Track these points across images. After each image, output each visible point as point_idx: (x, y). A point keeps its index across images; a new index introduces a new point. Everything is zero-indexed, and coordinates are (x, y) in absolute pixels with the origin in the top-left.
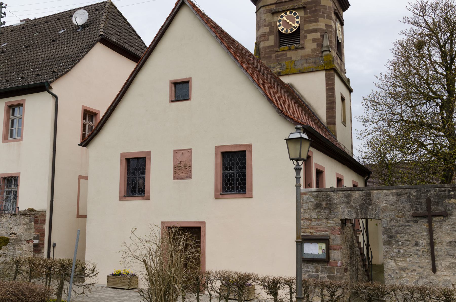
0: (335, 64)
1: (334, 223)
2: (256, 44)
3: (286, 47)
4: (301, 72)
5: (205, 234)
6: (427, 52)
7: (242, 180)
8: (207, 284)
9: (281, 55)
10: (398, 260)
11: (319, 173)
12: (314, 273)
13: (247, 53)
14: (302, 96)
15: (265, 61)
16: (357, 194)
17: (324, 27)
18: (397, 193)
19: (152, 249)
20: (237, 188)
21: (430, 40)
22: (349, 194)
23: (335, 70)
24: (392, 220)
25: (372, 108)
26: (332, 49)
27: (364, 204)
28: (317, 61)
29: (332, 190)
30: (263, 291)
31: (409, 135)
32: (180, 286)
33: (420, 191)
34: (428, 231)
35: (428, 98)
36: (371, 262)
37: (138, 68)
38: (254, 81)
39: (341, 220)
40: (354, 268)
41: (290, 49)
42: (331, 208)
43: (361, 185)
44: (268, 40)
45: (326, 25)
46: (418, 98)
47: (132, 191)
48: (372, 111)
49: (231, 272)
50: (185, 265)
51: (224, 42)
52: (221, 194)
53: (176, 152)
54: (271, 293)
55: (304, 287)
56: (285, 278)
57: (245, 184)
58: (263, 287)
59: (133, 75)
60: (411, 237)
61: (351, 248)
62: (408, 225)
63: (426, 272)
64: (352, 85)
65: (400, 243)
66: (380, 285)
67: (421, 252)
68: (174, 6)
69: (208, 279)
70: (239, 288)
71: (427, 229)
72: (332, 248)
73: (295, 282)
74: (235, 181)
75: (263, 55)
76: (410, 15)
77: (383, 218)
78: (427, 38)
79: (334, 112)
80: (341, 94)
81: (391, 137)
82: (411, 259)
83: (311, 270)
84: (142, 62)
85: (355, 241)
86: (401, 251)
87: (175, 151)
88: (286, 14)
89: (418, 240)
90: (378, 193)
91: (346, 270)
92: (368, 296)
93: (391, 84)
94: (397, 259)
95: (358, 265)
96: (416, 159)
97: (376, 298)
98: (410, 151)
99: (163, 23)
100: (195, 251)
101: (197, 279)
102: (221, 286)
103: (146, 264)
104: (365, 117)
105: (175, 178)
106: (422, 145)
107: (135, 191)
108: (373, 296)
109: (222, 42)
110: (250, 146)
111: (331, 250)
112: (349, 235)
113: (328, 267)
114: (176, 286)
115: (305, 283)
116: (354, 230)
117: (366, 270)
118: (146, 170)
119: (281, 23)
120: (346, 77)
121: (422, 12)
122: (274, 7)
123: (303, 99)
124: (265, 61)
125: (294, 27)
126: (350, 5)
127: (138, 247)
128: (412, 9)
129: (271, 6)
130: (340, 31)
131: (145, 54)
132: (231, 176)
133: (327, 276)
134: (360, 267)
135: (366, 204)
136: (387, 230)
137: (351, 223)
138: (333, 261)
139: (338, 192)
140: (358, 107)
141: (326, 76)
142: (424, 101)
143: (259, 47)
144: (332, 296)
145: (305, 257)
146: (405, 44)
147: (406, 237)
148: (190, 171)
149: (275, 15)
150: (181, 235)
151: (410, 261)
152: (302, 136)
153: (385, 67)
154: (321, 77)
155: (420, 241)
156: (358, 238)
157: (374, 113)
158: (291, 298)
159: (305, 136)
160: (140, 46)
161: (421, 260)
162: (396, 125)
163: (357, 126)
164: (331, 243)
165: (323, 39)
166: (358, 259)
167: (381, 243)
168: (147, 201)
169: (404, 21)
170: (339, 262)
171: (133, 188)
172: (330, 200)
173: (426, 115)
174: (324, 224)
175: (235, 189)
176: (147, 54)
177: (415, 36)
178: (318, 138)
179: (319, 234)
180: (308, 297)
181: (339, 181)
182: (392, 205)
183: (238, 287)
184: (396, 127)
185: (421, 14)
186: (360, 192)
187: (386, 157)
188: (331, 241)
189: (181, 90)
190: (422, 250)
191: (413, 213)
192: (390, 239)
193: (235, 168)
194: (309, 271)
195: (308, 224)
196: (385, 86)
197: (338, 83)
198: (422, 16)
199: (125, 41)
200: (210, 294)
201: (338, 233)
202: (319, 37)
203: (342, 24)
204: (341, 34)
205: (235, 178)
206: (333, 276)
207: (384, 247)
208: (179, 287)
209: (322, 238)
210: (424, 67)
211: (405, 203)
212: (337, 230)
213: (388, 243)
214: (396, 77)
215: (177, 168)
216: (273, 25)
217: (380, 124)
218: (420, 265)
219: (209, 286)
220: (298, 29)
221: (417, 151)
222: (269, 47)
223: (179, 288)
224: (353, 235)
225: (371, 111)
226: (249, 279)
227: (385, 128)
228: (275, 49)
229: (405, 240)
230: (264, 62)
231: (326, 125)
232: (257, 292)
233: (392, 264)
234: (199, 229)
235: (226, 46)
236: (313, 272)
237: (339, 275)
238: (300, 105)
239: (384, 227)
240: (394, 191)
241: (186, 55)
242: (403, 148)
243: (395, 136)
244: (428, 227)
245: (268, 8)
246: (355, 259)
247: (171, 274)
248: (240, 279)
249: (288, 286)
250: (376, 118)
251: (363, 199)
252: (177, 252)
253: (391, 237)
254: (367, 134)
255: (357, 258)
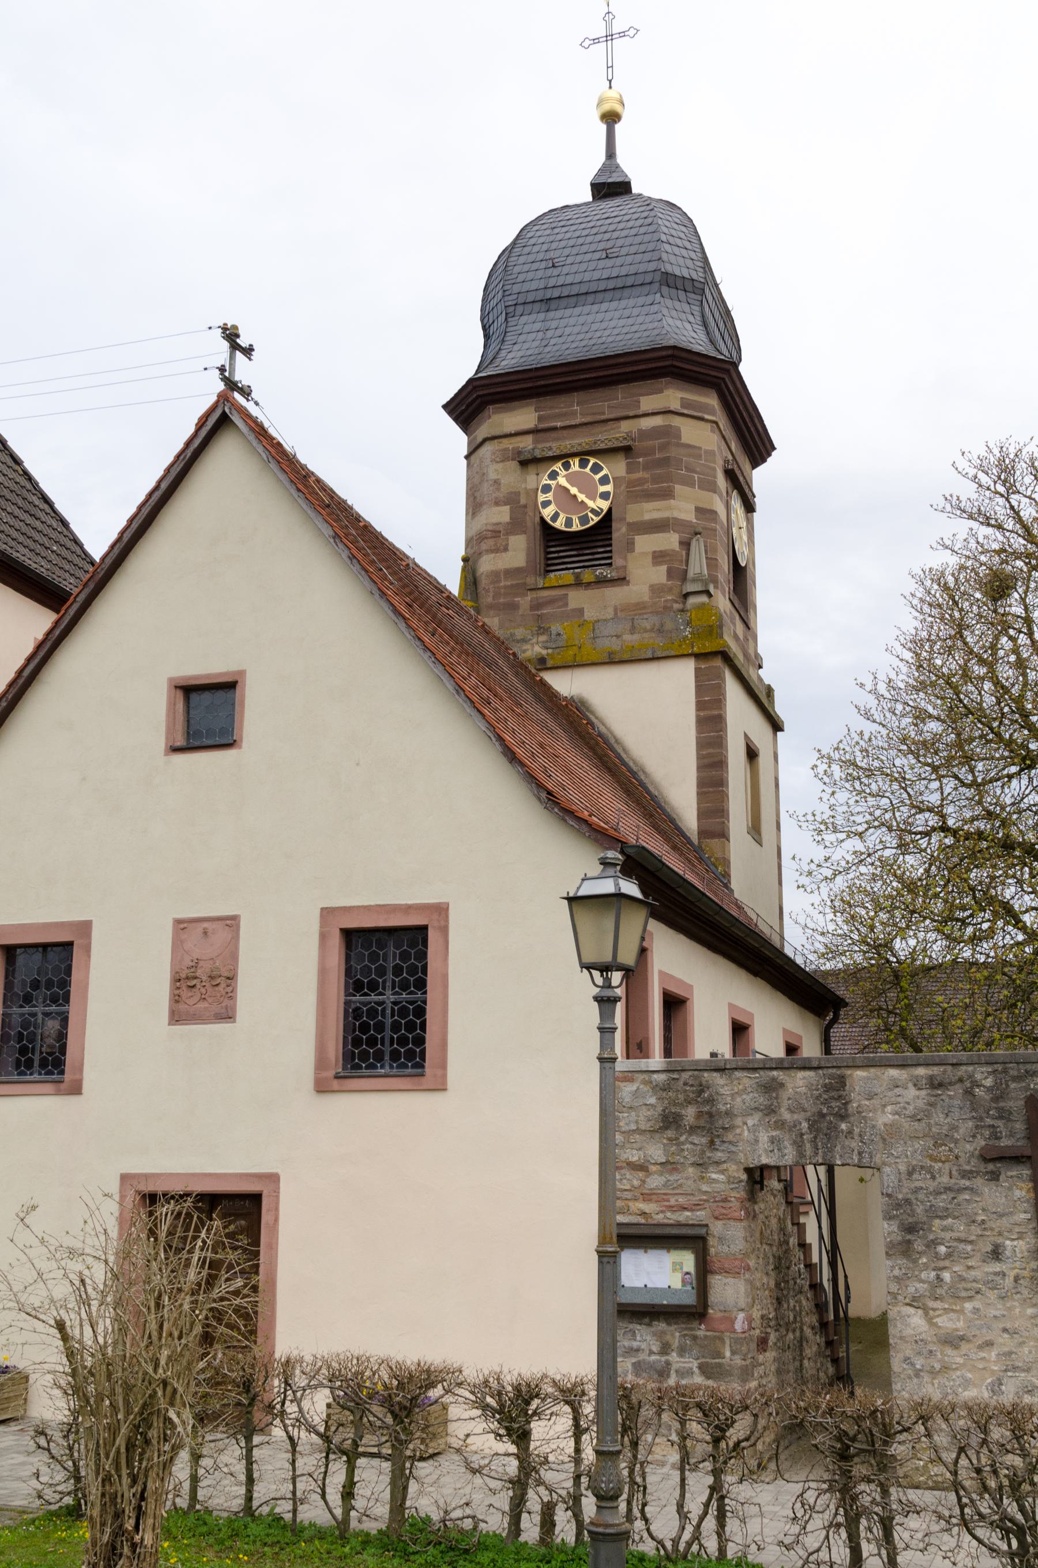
0: (726, 637)
1: (724, 1180)
2: (465, 560)
3: (567, 577)
4: (613, 660)
5: (276, 1220)
6: (1019, 610)
7: (411, 1027)
8: (283, 1404)
9: (552, 601)
10: (934, 1310)
11: (674, 1004)
12: (653, 1358)
13: (435, 591)
14: (617, 741)
15: (496, 620)
16: (799, 1082)
17: (690, 517)
18: (931, 1078)
19: (88, 1281)
20: (395, 1056)
21: (1030, 572)
22: (774, 1079)
23: (726, 657)
24: (914, 1169)
25: (847, 785)
26: (716, 587)
27: (823, 1116)
28: (669, 625)
29: (716, 1066)
30: (480, 1426)
31: (966, 880)
32: (187, 1414)
33: (1005, 1071)
34: (1032, 1209)
35: (1024, 759)
36: (846, 1313)
37: (57, 632)
38: (459, 689)
39: (748, 1171)
40: (791, 1336)
41: (578, 584)
42: (713, 1126)
43: (811, 1048)
44: (506, 549)
45: (699, 510)
46: (993, 758)
47: (18, 1064)
48: (847, 795)
49: (368, 1359)
50: (207, 1339)
51: (359, 556)
52: (337, 1077)
53: (181, 925)
54: (509, 1435)
55: (621, 1409)
56: (558, 1377)
57: (420, 1041)
58: (479, 1412)
59: (41, 654)
60: (976, 1230)
61: (781, 1265)
62: (966, 1189)
63: (1026, 1350)
64: (780, 708)
65: (942, 1249)
66: (879, 1402)
67: (1009, 1282)
68: (192, 430)
69: (287, 1383)
70: (395, 1416)
71: (1028, 1201)
72: (716, 1266)
73: (593, 1393)
74: (388, 1032)
75: (490, 600)
76: (967, 491)
77: (884, 1164)
78: (1019, 563)
79: (723, 797)
80: (746, 736)
81: (911, 887)
82: (977, 1304)
83: (644, 1346)
84: (72, 612)
85: (793, 1241)
86: (946, 1276)
87: (178, 922)
88: (567, 466)
89: (1000, 1240)
90: (868, 1078)
91: (762, 1344)
92: (839, 1439)
93: (908, 709)
94: (931, 1304)
95: (802, 1324)
96: (988, 956)
97: (865, 1447)
98: (970, 930)
99: (152, 484)
100: (245, 1286)
101: (247, 1386)
102: (329, 1406)
103: (65, 1338)
104: (825, 817)
105: (176, 1017)
106: (1011, 915)
107: (29, 1064)
108: (854, 1439)
109: (352, 557)
110: (441, 910)
111: (712, 1272)
112: (774, 1221)
113: (701, 1333)
114: (172, 1414)
115: (626, 1397)
116: (789, 1203)
117: (829, 1343)
118: (73, 989)
119: (550, 496)
120: (760, 679)
121: (1005, 482)
122: (526, 443)
123: (620, 751)
124: (496, 620)
125: (593, 511)
126: (774, 448)
127: (40, 1274)
128: (972, 472)
129: (519, 439)
130: (744, 531)
131: (85, 585)
132: (372, 1013)
133: (700, 1367)
134: (808, 1331)
135: (831, 1116)
136: (898, 1206)
137: (780, 1181)
138: (719, 1315)
139: (738, 1074)
140: (799, 779)
141: (696, 677)
142: (1014, 769)
143: (474, 572)
144: (716, 1441)
145: (624, 1298)
146: (951, 580)
147: (961, 1228)
148: (231, 996)
149: (532, 469)
150: (197, 1230)
151: (976, 1310)
152: (624, 890)
153: (888, 655)
154: (682, 675)
155: (1008, 1242)
156: (801, 1228)
157: (851, 802)
158: (578, 1450)
159: (631, 888)
160: (64, 553)
161: (1010, 1309)
162: (923, 843)
163: (797, 843)
164: (712, 1251)
165: (688, 555)
166: (804, 1302)
167: (879, 1248)
168: (73, 1100)
169: (948, 508)
170: (741, 1316)
171: (23, 1051)
172: (711, 1101)
173: (1020, 812)
174: (690, 1182)
175: (387, 1057)
176: (91, 586)
177: (983, 558)
178: (676, 889)
179: (672, 1217)
180: (635, 1444)
181: (739, 1030)
182: (915, 1118)
183: (392, 1412)
184: (925, 850)
185: (1001, 489)
186: (811, 1073)
187: (891, 949)
188: (712, 1241)
189: (206, 713)
190: (1012, 1274)
191: (982, 1148)
192: (908, 1237)
193: (389, 984)
194: (638, 1350)
195: (636, 1183)
196: (888, 715)
197: (733, 690)
198: (1002, 496)
199: (15, 534)
200: (291, 1438)
201: (736, 1214)
202: (676, 546)
203: (749, 507)
204: (745, 538)
205: (388, 1021)
206: (720, 1365)
207: (889, 1263)
208: (182, 1418)
209: (684, 1231)
210: (1013, 658)
211: (956, 1114)
212: (735, 1204)
213: (903, 1249)
214: (921, 687)
215: (183, 985)
216: (523, 501)
217: (874, 837)
218: (1008, 1326)
219: (289, 1410)
220: (607, 519)
221: (991, 932)
222: (509, 573)
223: (183, 1423)
224: (784, 1220)
225: (842, 796)
226: (432, 1385)
227: (888, 853)
228: (530, 580)
229: (960, 1240)
230: (493, 622)
231: (695, 839)
232: (457, 1430)
233: (916, 1321)
234: (256, 1198)
235: (367, 571)
236: (651, 1353)
237: (738, 1361)
238: (609, 770)
239: (889, 1196)
240: (921, 1071)
241: (229, 591)
242: (945, 921)
243: (920, 880)
244: (1032, 1195)
245: (509, 444)
246: (792, 1303)
247: (155, 1370)
248: (401, 1386)
249: (567, 1409)
250: (859, 819)
251: (817, 1098)
252: (180, 1290)
253: (911, 1229)
254: (829, 873)
255: (799, 1302)
